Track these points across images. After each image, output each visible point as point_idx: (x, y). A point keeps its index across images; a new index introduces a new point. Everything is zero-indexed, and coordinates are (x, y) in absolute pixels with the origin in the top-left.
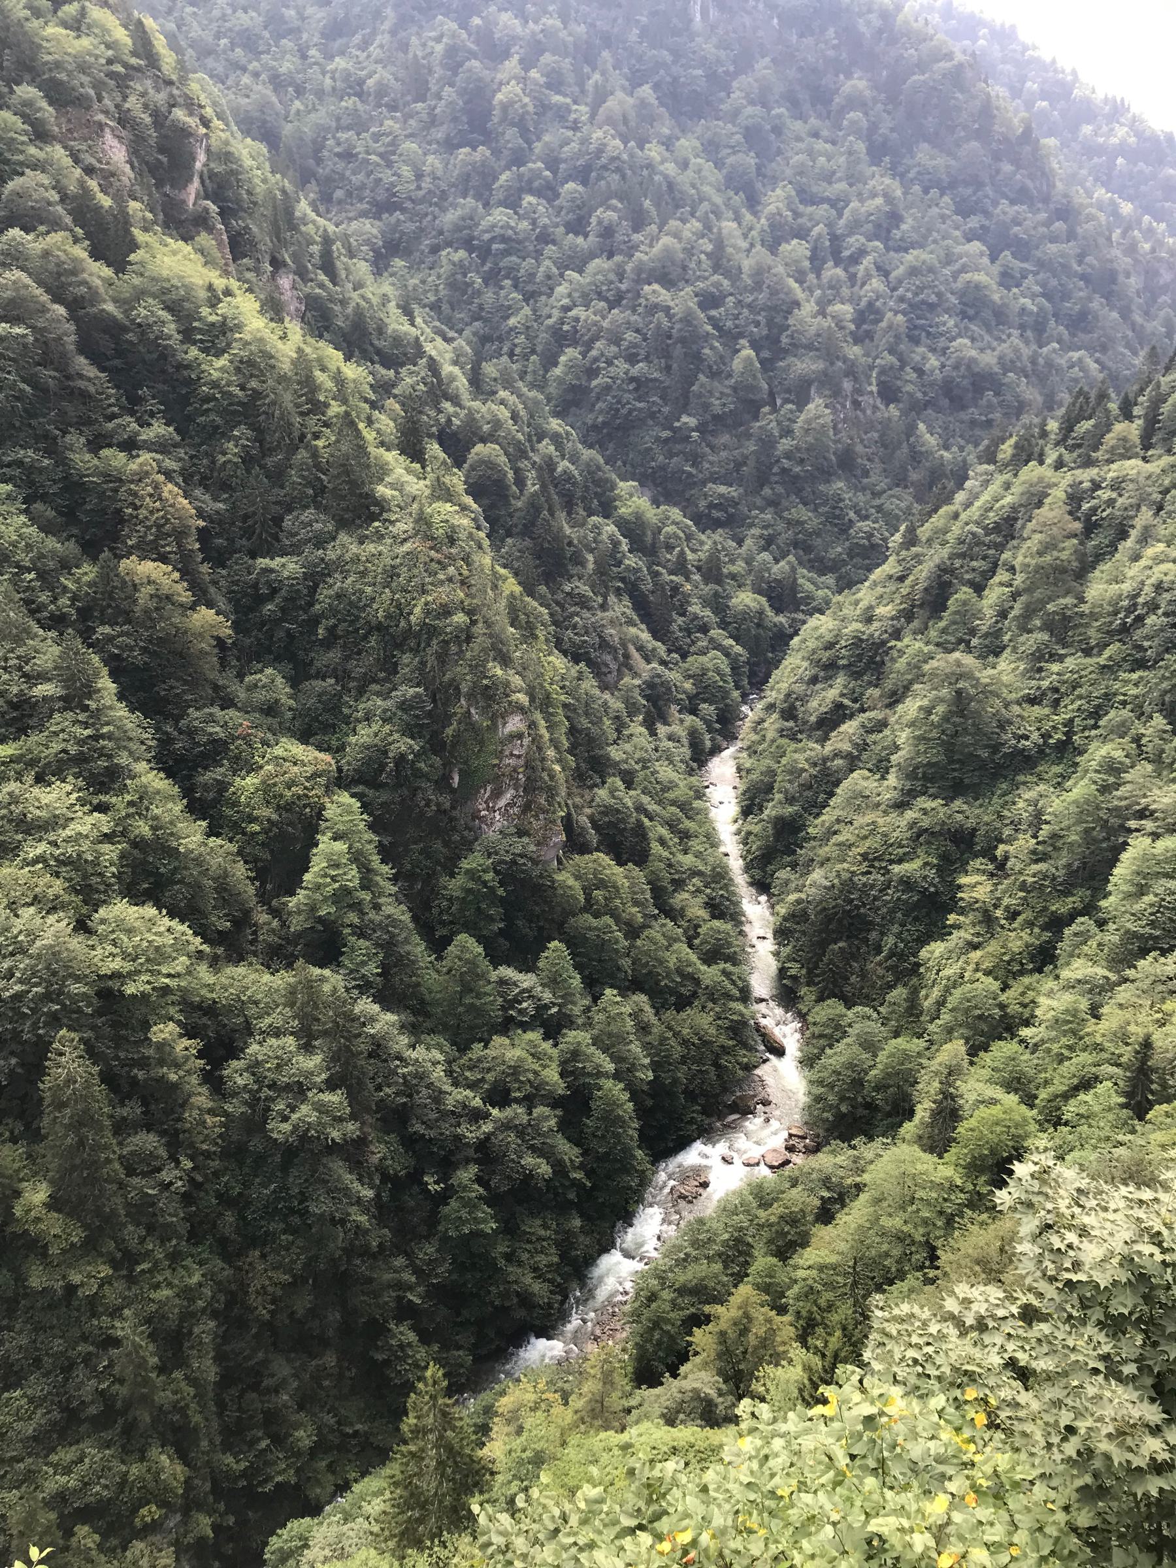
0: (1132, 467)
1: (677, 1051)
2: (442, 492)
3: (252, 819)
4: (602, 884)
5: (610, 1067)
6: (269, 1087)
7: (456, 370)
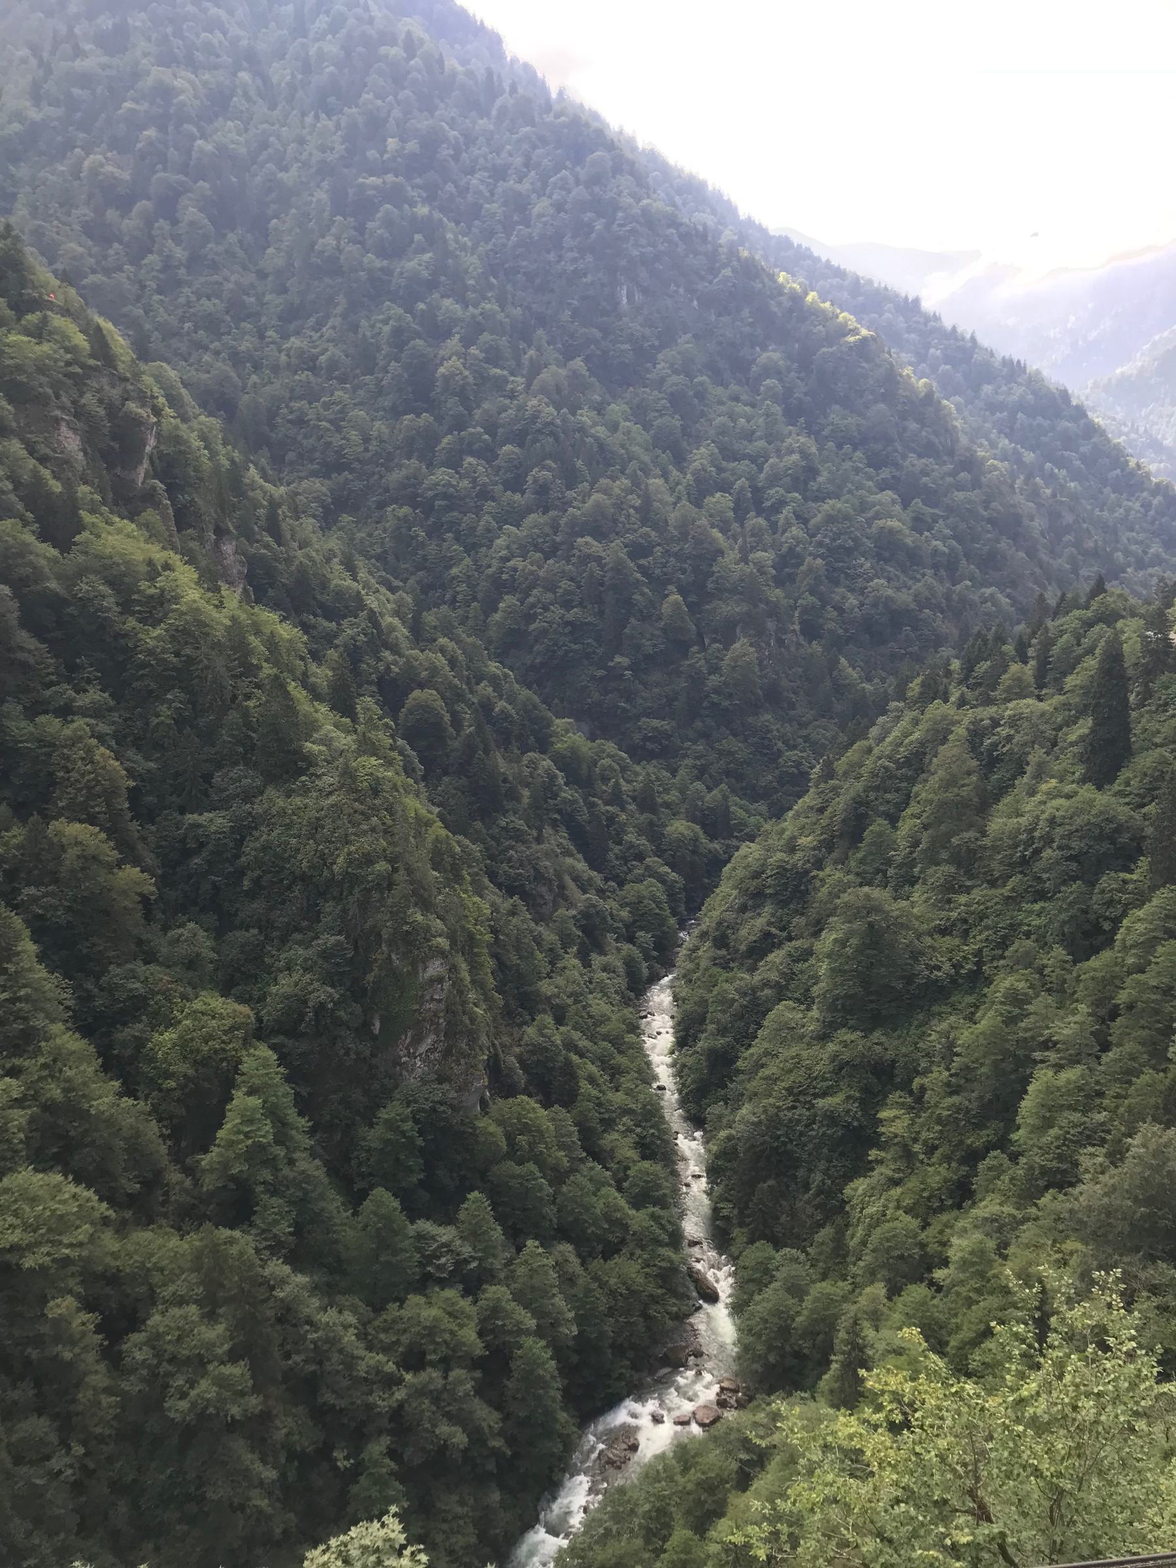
0: (1028, 705)
1: (603, 1303)
2: (367, 747)
3: (168, 1075)
4: (525, 1129)
5: (531, 1323)
6: (170, 1361)
7: (396, 621)
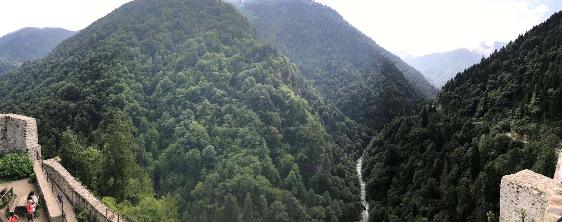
2: (316, 120)
4: (336, 181)
5: (334, 213)
